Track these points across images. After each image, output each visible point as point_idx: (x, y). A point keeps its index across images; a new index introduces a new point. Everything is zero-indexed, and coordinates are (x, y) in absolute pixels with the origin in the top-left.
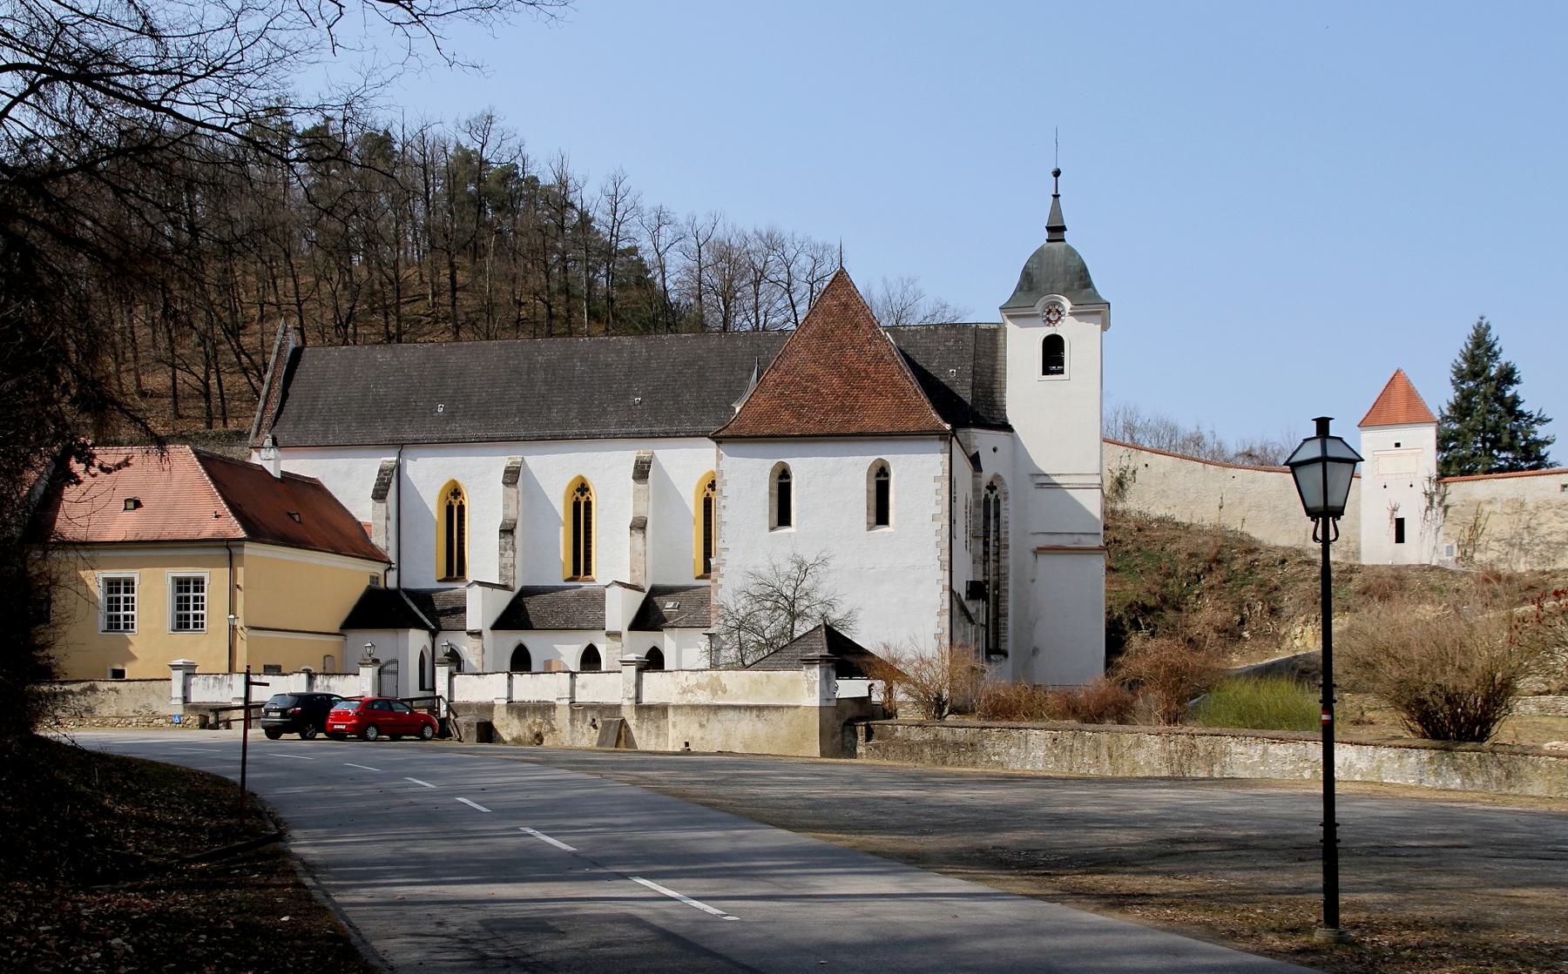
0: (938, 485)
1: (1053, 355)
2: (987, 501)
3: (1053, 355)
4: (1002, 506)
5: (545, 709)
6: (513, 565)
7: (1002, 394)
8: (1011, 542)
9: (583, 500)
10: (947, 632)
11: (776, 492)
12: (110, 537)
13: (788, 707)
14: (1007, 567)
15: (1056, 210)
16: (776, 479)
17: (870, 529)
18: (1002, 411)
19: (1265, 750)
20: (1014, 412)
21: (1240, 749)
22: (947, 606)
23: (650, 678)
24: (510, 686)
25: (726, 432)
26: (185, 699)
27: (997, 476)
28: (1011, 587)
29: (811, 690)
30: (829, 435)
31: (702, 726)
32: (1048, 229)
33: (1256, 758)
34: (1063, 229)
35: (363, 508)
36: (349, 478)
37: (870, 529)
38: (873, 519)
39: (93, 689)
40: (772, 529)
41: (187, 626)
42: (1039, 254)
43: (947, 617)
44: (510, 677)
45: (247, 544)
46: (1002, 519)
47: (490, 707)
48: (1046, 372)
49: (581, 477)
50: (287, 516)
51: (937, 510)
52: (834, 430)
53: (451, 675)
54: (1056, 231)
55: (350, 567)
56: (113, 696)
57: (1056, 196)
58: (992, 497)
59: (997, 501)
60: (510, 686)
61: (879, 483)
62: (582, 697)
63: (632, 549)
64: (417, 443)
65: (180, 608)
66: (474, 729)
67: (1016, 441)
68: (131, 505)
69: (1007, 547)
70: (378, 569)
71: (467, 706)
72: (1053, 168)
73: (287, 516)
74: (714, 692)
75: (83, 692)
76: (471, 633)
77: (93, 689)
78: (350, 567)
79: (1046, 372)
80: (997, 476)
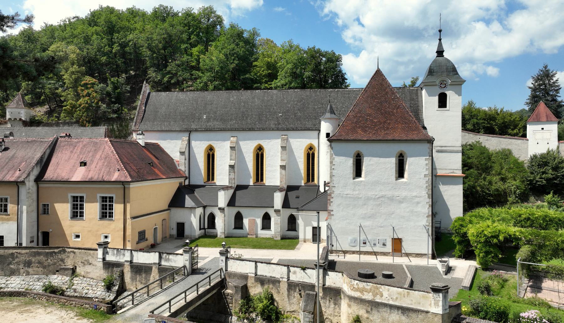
0: (427, 162)
1: (443, 102)
3: (443, 102)
5: (275, 282)
6: (234, 179)
9: (260, 153)
10: (431, 224)
12: (73, 179)
15: (440, 45)
16: (355, 158)
17: (396, 180)
26: (104, 259)
30: (380, 140)
35: (175, 155)
36: (173, 147)
37: (396, 180)
39: (64, 251)
40: (354, 179)
42: (435, 61)
47: (245, 277)
48: (440, 107)
49: (259, 144)
50: (148, 163)
51: (427, 173)
52: (381, 138)
56: (72, 255)
61: (399, 160)
62: (293, 278)
63: (281, 173)
64: (196, 130)
66: (240, 289)
68: (83, 164)
70: (182, 180)
72: (439, 29)
74: (375, 295)
75: (60, 252)
76: (220, 209)
77: (64, 251)
79: (440, 107)
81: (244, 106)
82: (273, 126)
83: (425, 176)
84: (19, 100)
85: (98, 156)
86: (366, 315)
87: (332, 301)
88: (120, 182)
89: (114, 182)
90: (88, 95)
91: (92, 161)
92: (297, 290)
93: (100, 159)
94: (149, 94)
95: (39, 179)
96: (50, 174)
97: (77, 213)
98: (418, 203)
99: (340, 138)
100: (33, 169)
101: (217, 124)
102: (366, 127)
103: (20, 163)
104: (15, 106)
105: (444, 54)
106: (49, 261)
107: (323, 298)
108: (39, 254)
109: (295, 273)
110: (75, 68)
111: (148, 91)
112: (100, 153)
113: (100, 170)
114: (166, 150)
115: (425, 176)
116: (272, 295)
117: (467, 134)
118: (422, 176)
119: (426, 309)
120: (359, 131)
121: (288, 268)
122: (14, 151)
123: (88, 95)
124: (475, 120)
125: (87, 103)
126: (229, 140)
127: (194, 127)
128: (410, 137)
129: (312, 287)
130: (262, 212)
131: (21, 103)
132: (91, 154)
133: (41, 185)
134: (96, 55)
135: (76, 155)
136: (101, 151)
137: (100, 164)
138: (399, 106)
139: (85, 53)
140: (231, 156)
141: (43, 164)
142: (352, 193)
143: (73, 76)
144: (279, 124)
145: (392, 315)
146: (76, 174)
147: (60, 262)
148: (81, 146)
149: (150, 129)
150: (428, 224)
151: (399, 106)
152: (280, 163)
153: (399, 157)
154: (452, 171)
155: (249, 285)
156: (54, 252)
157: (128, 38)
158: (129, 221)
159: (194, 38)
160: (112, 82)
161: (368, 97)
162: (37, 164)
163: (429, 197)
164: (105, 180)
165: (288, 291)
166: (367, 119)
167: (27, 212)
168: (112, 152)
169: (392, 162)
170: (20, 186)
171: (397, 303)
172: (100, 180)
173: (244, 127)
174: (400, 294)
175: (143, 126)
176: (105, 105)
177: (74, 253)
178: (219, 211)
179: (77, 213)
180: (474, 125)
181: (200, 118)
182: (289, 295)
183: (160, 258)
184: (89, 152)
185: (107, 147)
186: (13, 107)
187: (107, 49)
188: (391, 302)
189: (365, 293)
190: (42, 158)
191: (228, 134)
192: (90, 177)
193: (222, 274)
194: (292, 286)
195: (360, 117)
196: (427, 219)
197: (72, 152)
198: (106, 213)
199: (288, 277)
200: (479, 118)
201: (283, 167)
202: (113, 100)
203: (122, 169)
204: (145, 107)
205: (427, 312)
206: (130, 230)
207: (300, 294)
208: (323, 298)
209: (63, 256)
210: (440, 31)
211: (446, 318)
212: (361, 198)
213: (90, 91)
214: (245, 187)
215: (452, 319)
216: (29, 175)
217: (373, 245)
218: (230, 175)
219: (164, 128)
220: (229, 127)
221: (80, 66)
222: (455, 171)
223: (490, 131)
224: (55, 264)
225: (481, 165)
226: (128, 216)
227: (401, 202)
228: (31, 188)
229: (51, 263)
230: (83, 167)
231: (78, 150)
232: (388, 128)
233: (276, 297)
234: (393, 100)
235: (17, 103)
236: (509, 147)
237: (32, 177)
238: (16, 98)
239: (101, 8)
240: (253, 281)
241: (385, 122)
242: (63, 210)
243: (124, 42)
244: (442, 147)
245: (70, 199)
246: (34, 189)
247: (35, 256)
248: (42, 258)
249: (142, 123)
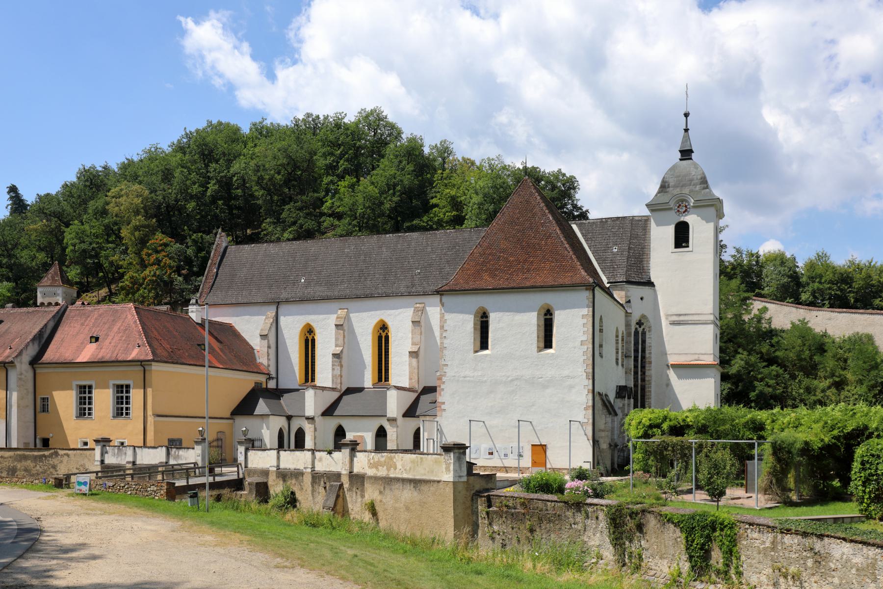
0: (585, 321)
1: (682, 236)
2: (636, 332)
3: (682, 236)
4: (647, 336)
5: (298, 474)
6: (341, 376)
7: (648, 262)
8: (653, 360)
9: (384, 335)
10: (591, 421)
11: (479, 327)
13: (434, 481)
14: (650, 376)
16: (479, 319)
18: (647, 273)
19: (775, 537)
20: (655, 274)
21: (756, 535)
22: (590, 403)
23: (833, 390)
24: (278, 458)
25: (446, 288)
26: (102, 462)
27: (643, 316)
28: (653, 389)
29: (448, 469)
30: (513, 288)
31: (381, 492)
32: (681, 151)
33: (768, 544)
34: (691, 151)
35: (255, 342)
36: (251, 326)
37: (540, 350)
38: (542, 345)
39: (57, 454)
40: (476, 352)
41: (122, 414)
43: (590, 411)
44: (278, 453)
45: (153, 363)
46: (647, 344)
47: (266, 473)
49: (382, 321)
51: (584, 338)
52: (515, 285)
53: (247, 450)
54: (686, 154)
55: (242, 377)
56: (65, 458)
57: (686, 130)
58: (640, 330)
59: (644, 333)
60: (278, 458)
61: (546, 320)
62: (320, 467)
63: (410, 364)
64: (287, 301)
65: (80, 403)
67: (655, 291)
68: (93, 340)
69: (650, 363)
71: (254, 472)
73: (184, 346)
75: (51, 456)
76: (308, 418)
77: (57, 454)
78: (242, 377)
80: (643, 316)
81: (364, 261)
82: (403, 290)
83: (582, 343)
84: (56, 273)
85: (115, 329)
86: (379, 498)
87: (359, 493)
88: (138, 361)
89: (130, 361)
90: (158, 262)
91: (107, 335)
92: (322, 483)
93: (118, 332)
94: (226, 248)
95: (35, 362)
96: (50, 355)
97: (84, 409)
98: (571, 387)
99: (454, 288)
100: (27, 346)
101: (320, 290)
102: (496, 269)
103: (13, 340)
104: (49, 283)
105: (693, 156)
106: (38, 467)
107: (350, 490)
108: (25, 458)
109: (321, 460)
110: (140, 220)
111: (224, 245)
112: (118, 325)
113: (115, 347)
114: (243, 335)
115: (582, 343)
116: (293, 493)
117: (794, 309)
118: (578, 343)
119: (438, 479)
120: (486, 276)
121: (313, 454)
122: (9, 324)
123: (158, 262)
124: (816, 285)
125: (154, 275)
126: (336, 313)
127: (284, 295)
128: (561, 281)
129: (338, 476)
130: (375, 424)
131: (58, 278)
132: (106, 326)
133: (38, 371)
134: (177, 200)
135: (87, 328)
136: (121, 322)
137: (117, 339)
138: (551, 234)
139: (160, 198)
140: (337, 339)
141: (43, 341)
142: (472, 375)
143: (137, 233)
144: (413, 286)
145: (405, 492)
146: (83, 353)
147: (51, 470)
148: (96, 316)
149: (220, 302)
150: (586, 421)
151: (551, 234)
152: (410, 348)
153: (546, 315)
154: (696, 357)
155: (270, 483)
156: (44, 456)
157: (232, 170)
158: (151, 419)
159: (343, 165)
160: (194, 240)
161: (505, 223)
162: (33, 340)
163: (588, 378)
164: (120, 359)
165: (313, 486)
166: (500, 257)
167: (18, 407)
168: (135, 322)
169: (531, 321)
170: (9, 369)
171: (410, 476)
172: (113, 359)
173: (359, 293)
174: (413, 462)
175: (211, 299)
176: (181, 279)
177: (68, 455)
178: (306, 421)
179: (84, 409)
180: (813, 293)
181: (295, 282)
182: (313, 491)
183: (168, 454)
184: (105, 323)
185: (129, 316)
186: (46, 284)
187: (195, 189)
188: (405, 476)
189: (380, 468)
190: (41, 333)
191: (334, 305)
192: (100, 356)
193: (241, 472)
194: (316, 477)
195: (490, 254)
196: (584, 412)
197: (82, 324)
198: (121, 409)
199: (313, 467)
200: (823, 281)
201: (414, 354)
202: (195, 269)
203: (144, 345)
204: (218, 269)
205: (439, 482)
206: (152, 433)
207: (325, 488)
208: (350, 490)
209: (55, 461)
210: (686, 115)
211: (460, 487)
212: (485, 382)
213: (160, 256)
214: (360, 390)
215: (473, 492)
216: (20, 354)
217: (503, 457)
218: (333, 369)
219: (240, 300)
220: (336, 293)
221: (148, 217)
222: (702, 357)
223: (840, 302)
224: (44, 472)
225: (801, 360)
226: (150, 412)
227: (545, 387)
228: (24, 372)
229: (41, 470)
230: (94, 344)
231: (91, 321)
232: (528, 270)
233: (298, 496)
234: (542, 225)
235: (53, 278)
236: (869, 331)
237: (26, 358)
238: (52, 271)
239: (210, 124)
240: (274, 477)
241: (525, 261)
242: (65, 401)
243: (225, 176)
244: (680, 315)
245: (74, 387)
246: (30, 374)
247: (20, 461)
248: (29, 463)
249: (211, 294)
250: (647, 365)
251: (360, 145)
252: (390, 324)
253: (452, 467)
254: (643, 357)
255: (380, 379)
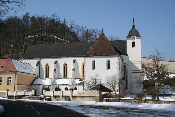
2: (124, 66)
3: (134, 45)
14: (128, 76)
18: (126, 52)
29: (98, 94)
37: (107, 70)
38: (108, 68)
40: (107, 70)
57: (133, 22)
62: (64, 95)
68: (2, 67)
69: (128, 72)
115: (117, 68)
129: (69, 96)
199: (53, 95)
210: (133, 19)
250: (127, 73)
251: (38, 22)
252: (67, 64)
253: (99, 93)
254: (126, 71)
255: (65, 76)
